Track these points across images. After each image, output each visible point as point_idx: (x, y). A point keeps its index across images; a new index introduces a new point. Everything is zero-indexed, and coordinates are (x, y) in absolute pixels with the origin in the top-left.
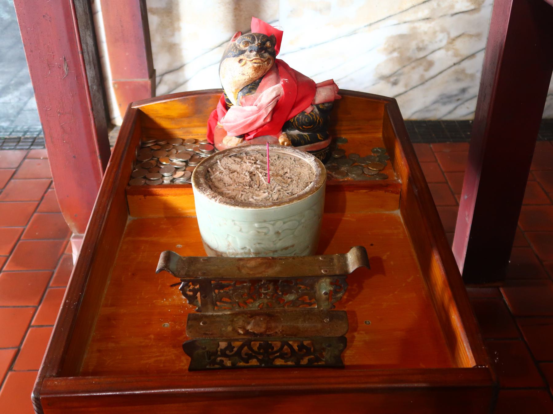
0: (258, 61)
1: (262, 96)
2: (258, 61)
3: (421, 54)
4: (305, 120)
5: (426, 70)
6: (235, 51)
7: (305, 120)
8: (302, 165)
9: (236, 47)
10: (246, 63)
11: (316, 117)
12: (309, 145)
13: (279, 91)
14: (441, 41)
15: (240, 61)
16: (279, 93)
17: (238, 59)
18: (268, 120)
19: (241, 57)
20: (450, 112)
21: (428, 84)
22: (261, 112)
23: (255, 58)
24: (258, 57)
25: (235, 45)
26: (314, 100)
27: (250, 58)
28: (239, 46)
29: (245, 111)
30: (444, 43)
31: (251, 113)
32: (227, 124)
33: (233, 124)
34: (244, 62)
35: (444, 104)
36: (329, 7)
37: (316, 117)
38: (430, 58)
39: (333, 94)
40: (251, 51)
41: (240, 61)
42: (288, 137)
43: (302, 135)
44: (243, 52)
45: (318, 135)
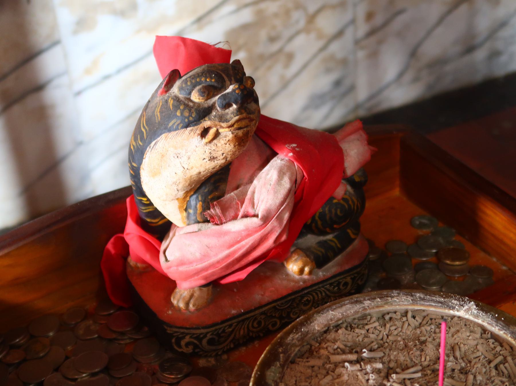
0: (243, 123)
1: (254, 193)
2: (243, 123)
3: (275, 47)
4: (336, 214)
5: (287, 65)
6: (186, 114)
7: (336, 214)
8: (450, 321)
9: (186, 106)
10: (217, 135)
11: (353, 201)
12: (339, 258)
13: (292, 174)
14: (297, 22)
15: (204, 133)
16: (294, 178)
17: (199, 128)
18: (284, 238)
19: (207, 123)
20: (326, 117)
21: (292, 87)
22: (269, 226)
23: (237, 118)
24: (244, 115)
25: (176, 99)
26: (344, 171)
27: (227, 121)
28: (190, 100)
29: (226, 233)
30: (302, 23)
31: (244, 234)
32: (182, 269)
33: (200, 266)
34: (212, 132)
35: (317, 107)
36: (134, 7)
37: (353, 201)
38: (289, 48)
39: (366, 148)
40: (228, 105)
41: (204, 133)
42: (307, 256)
43: (325, 242)
44: (204, 113)
45: (349, 231)
